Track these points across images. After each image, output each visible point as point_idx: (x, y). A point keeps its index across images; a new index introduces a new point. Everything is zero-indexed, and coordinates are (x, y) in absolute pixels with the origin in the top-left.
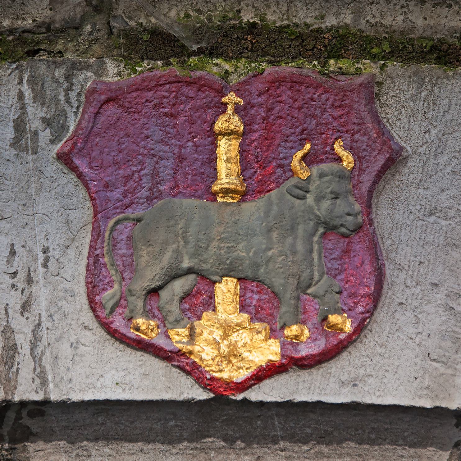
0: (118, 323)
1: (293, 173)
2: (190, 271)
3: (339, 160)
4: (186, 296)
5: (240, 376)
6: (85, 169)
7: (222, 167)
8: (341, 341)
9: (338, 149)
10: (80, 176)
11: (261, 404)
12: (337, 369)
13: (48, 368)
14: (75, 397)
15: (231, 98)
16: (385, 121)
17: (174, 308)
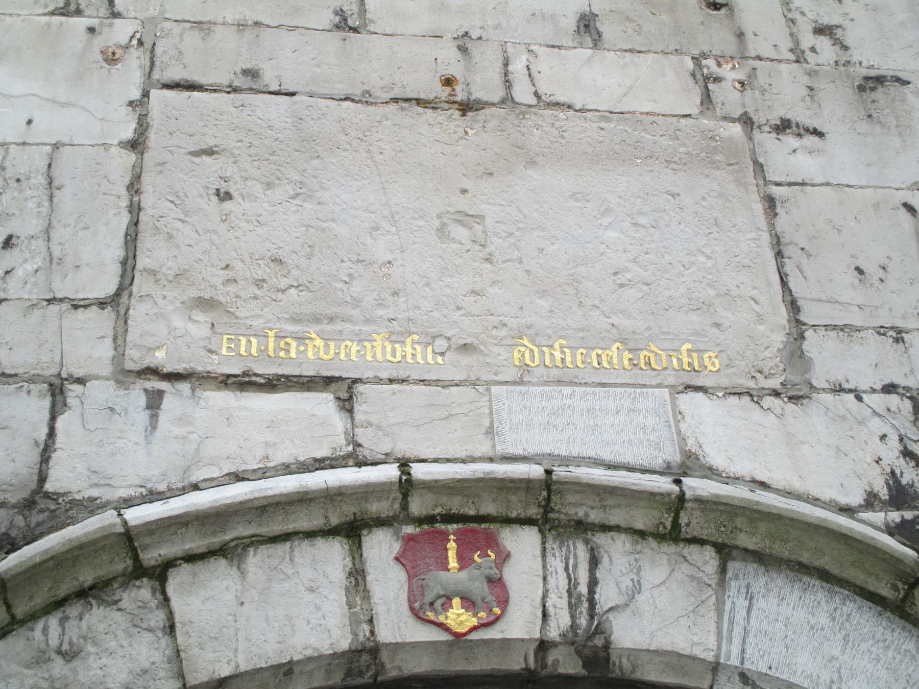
0: (421, 615)
1: (475, 561)
2: (443, 596)
3: (490, 556)
4: (443, 605)
5: (464, 630)
6: (404, 562)
7: (450, 560)
8: (428, 523)
9: (489, 552)
10: (403, 565)
11: (471, 640)
12: (315, 216)
13: (571, 573)
14: (407, 641)
15: (452, 537)
16: (555, 388)
17: (440, 608)
